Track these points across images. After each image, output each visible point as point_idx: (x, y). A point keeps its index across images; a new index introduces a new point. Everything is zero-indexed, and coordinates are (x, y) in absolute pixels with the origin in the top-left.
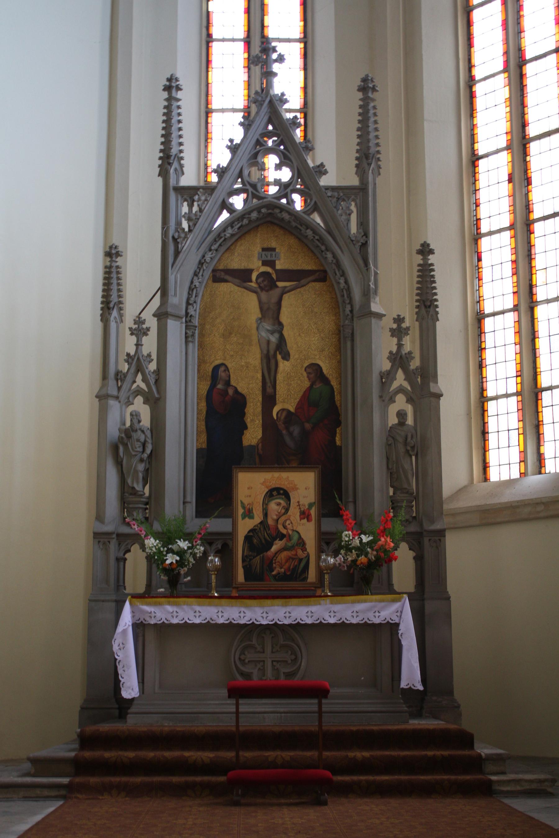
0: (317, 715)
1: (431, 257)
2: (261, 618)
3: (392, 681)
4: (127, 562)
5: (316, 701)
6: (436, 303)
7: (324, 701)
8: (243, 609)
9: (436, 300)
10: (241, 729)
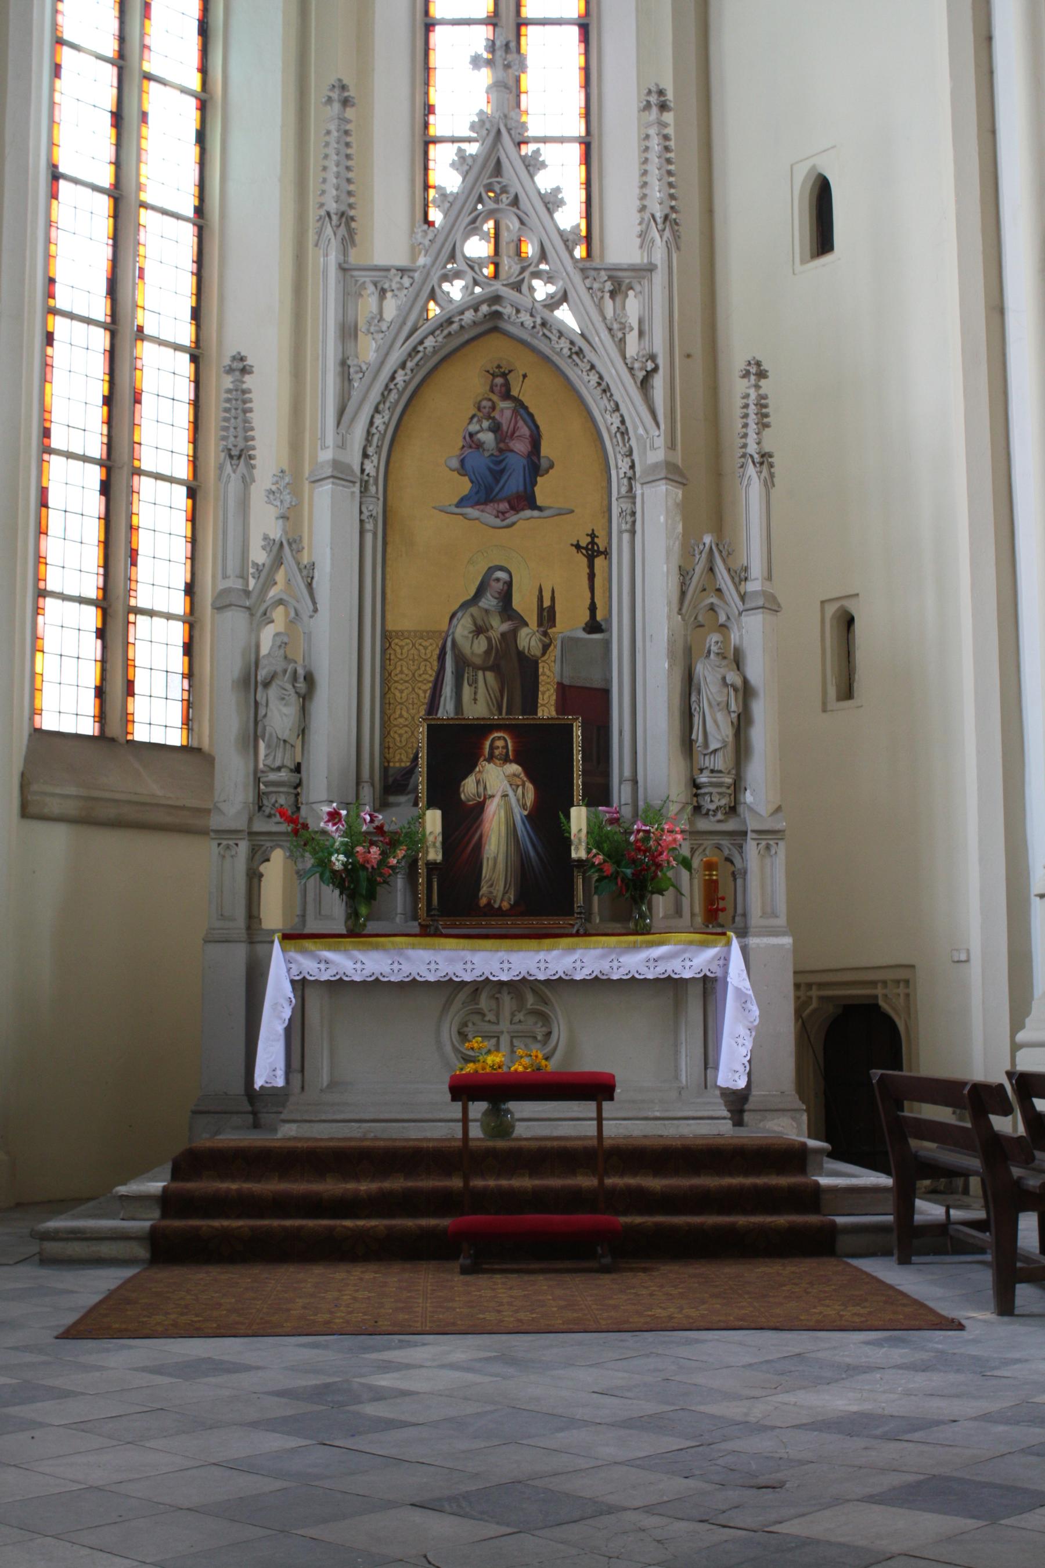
0: (595, 1122)
1: (247, 378)
2: (621, 970)
3: (706, 1068)
4: (263, 879)
5: (592, 1105)
6: (251, 452)
7: (606, 1105)
8: (397, 958)
9: (253, 448)
10: (607, 1143)
